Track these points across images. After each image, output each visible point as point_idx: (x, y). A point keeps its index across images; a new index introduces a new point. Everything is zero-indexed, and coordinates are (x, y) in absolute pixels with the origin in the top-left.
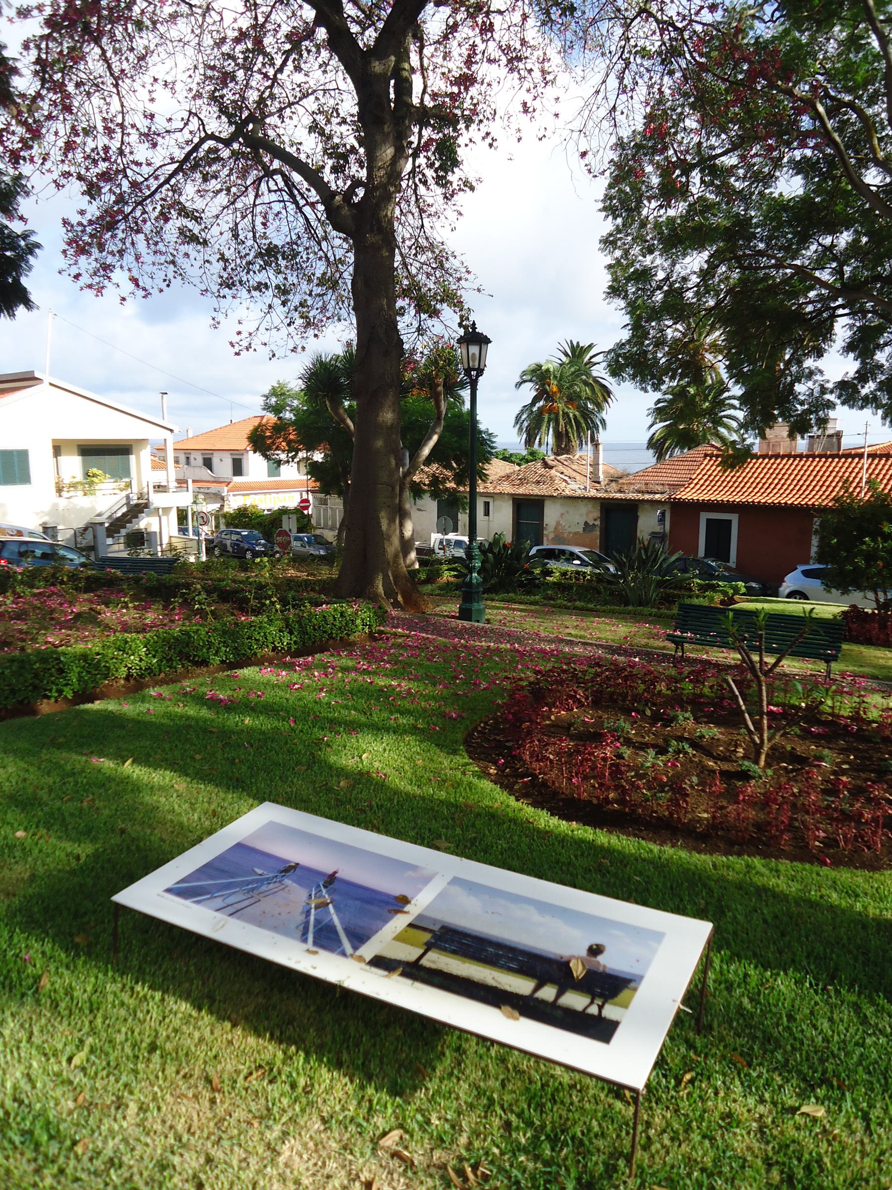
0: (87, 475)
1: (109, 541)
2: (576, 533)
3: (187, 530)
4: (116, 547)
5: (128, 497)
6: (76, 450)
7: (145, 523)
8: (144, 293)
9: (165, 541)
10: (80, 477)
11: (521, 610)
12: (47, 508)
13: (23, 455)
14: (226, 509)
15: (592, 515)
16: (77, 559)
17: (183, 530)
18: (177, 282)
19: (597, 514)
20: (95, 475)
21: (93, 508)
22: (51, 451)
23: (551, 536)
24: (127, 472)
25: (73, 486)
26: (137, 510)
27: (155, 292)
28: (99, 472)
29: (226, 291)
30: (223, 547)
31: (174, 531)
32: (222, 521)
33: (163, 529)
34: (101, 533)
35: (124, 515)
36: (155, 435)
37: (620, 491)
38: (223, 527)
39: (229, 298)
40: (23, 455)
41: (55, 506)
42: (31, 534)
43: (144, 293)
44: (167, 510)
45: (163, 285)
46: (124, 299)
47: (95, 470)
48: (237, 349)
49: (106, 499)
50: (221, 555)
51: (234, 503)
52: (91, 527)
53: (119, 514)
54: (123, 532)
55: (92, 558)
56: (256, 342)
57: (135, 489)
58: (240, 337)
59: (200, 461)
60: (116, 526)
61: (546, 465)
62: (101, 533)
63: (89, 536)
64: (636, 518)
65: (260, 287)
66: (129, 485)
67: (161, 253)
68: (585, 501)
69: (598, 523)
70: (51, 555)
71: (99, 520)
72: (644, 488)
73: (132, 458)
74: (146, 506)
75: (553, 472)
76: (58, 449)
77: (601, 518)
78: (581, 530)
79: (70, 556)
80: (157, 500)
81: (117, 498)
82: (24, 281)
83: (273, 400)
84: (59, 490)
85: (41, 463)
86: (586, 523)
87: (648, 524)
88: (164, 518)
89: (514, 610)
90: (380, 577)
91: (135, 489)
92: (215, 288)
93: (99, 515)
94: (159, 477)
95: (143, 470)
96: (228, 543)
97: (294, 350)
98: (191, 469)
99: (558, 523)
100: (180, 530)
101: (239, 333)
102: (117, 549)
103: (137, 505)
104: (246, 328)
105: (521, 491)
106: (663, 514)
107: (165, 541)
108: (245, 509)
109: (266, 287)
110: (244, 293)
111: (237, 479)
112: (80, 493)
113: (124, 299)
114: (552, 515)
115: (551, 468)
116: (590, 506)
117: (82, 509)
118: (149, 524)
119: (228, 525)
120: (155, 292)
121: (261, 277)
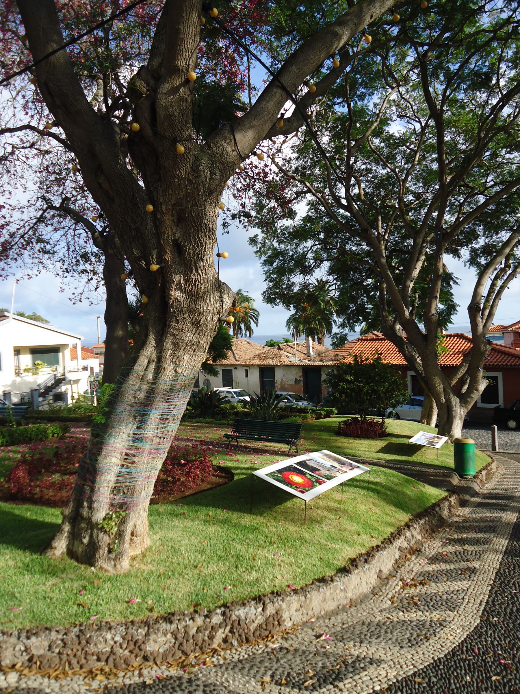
0: (34, 364)
2: (291, 385)
6: (29, 352)
8: (28, 277)
10: (30, 365)
11: (191, 426)
12: (9, 383)
15: (298, 374)
18: (43, 271)
19: (301, 374)
20: (38, 364)
21: (36, 382)
22: (12, 352)
23: (279, 387)
24: (57, 362)
25: (26, 370)
26: (58, 382)
29: (66, 274)
34: (36, 394)
35: (52, 385)
36: (71, 342)
37: (321, 361)
39: (69, 277)
41: (14, 381)
43: (28, 277)
45: (37, 273)
46: (18, 280)
47: (39, 362)
48: (73, 301)
49: (44, 376)
52: (32, 391)
56: (83, 297)
58: (74, 296)
60: (48, 389)
61: (280, 349)
62: (36, 394)
65: (84, 271)
67: (36, 258)
68: (295, 367)
69: (302, 379)
72: (333, 359)
73: (60, 354)
74: (64, 379)
75: (282, 352)
76: (18, 351)
77: (303, 376)
78: (294, 383)
84: (18, 374)
86: (296, 379)
89: (188, 426)
90: (435, 405)
92: (61, 273)
93: (39, 386)
99: (282, 379)
101: (74, 294)
102: (44, 405)
103: (59, 379)
105: (263, 363)
110: (76, 275)
113: (18, 280)
114: (279, 375)
115: (282, 350)
116: (297, 369)
117: (29, 382)
118: (67, 389)
120: (34, 276)
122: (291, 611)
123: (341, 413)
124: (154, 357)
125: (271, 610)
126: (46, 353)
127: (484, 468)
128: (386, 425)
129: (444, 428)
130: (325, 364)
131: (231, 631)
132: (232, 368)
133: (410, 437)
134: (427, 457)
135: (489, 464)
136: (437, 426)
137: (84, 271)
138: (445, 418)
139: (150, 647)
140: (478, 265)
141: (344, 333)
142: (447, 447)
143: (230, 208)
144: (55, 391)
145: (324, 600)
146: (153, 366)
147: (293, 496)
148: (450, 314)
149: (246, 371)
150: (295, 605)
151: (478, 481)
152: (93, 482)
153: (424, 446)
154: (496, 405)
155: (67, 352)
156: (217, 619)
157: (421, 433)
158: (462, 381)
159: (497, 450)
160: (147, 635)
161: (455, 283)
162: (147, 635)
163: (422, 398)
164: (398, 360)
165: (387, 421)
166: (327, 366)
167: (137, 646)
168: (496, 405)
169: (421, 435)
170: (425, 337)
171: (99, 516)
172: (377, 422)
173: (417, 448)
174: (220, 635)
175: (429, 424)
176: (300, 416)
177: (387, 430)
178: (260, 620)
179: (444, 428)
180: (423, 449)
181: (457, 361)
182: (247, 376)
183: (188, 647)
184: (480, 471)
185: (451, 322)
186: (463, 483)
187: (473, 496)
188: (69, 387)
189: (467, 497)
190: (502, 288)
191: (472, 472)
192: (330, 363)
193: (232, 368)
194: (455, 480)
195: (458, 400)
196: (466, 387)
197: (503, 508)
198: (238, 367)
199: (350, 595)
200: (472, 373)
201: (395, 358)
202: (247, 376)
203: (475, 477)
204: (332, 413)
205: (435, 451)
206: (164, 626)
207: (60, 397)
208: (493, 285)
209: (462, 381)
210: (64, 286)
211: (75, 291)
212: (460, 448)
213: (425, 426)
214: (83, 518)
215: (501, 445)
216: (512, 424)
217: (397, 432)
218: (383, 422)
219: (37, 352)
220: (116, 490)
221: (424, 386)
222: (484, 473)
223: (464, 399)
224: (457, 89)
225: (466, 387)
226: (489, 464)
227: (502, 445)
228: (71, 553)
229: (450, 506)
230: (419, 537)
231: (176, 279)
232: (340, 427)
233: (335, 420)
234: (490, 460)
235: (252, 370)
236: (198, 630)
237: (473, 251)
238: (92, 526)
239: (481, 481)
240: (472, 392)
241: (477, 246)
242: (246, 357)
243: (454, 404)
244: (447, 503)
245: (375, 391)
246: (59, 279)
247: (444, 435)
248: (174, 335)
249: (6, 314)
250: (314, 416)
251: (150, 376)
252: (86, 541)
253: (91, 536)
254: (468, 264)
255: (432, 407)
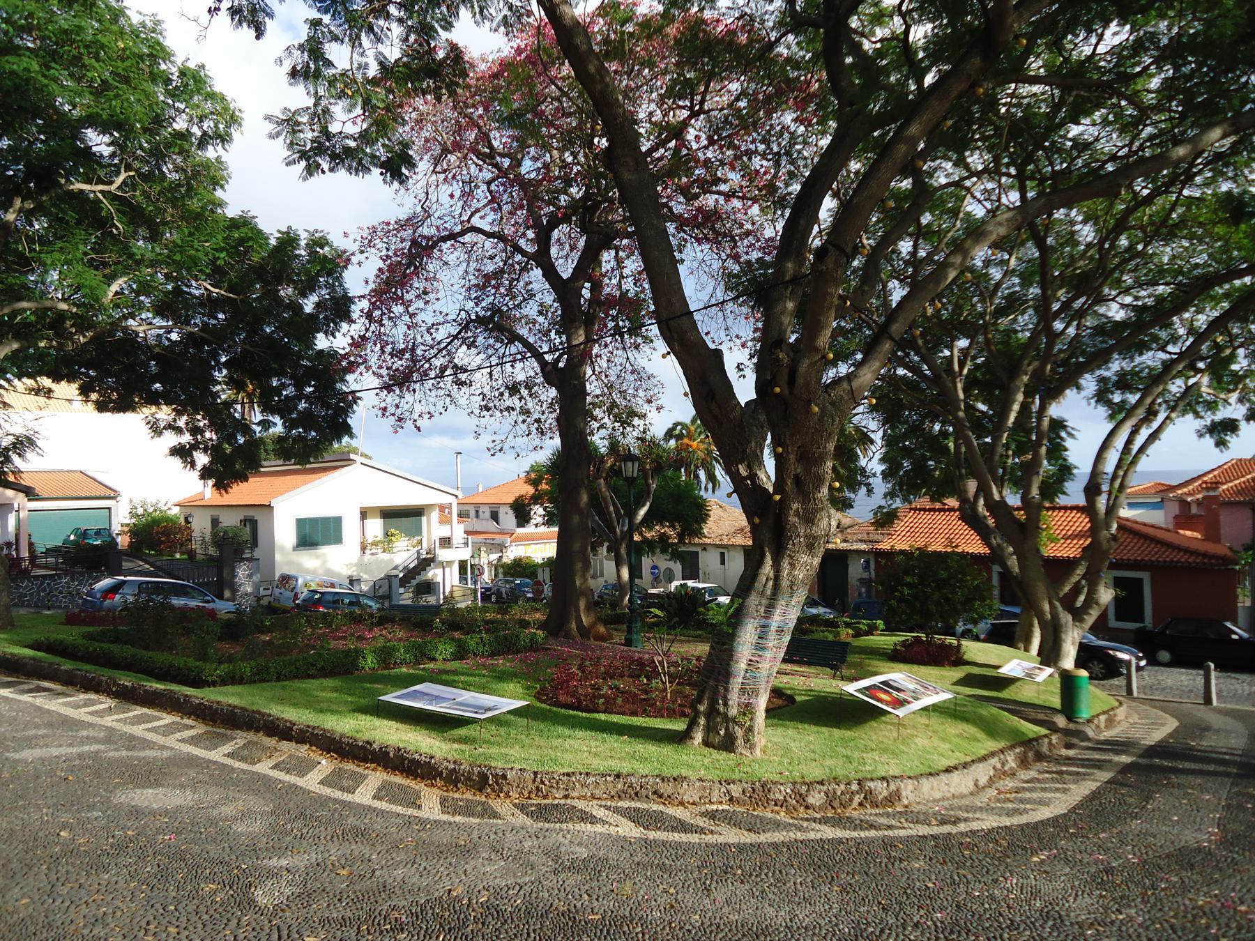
0: (386, 535)
1: (401, 590)
3: (466, 579)
4: (406, 596)
5: (418, 552)
7: (434, 574)
9: (448, 590)
10: (380, 537)
13: (337, 521)
14: (505, 560)
16: (375, 606)
17: (462, 578)
18: (451, 408)
24: (419, 532)
25: (375, 544)
27: (436, 414)
28: (396, 532)
30: (498, 593)
31: (456, 581)
32: (501, 570)
33: (447, 580)
34: (396, 582)
38: (501, 576)
40: (337, 521)
42: (341, 586)
44: (450, 563)
47: (393, 531)
49: (403, 554)
50: (497, 602)
51: (511, 554)
52: (389, 578)
53: (412, 565)
54: (414, 582)
55: (387, 604)
56: (506, 446)
57: (425, 546)
59: (488, 514)
60: (411, 574)
62: (396, 582)
63: (385, 588)
64: (847, 566)
65: (510, 409)
66: (420, 542)
70: (356, 601)
71: (395, 572)
72: (866, 538)
73: (424, 519)
74: (433, 560)
76: (364, 514)
79: (370, 603)
80: (443, 555)
81: (409, 553)
82: (349, 420)
83: (533, 476)
84: (363, 549)
85: (351, 529)
87: (856, 570)
88: (447, 570)
90: (1036, 622)
91: (425, 546)
92: (477, 412)
93: (396, 568)
94: (445, 531)
95: (433, 529)
96: (503, 590)
97: (535, 449)
98: (479, 521)
100: (460, 580)
102: (405, 597)
103: (425, 559)
104: (498, 438)
106: (867, 562)
107: (448, 590)
108: (520, 560)
109: (513, 409)
110: (498, 413)
111: (520, 531)
112: (380, 550)
118: (435, 575)
119: (505, 574)
120: (436, 414)
121: (509, 403)
122: (907, 789)
123: (890, 629)
124: (772, 575)
125: (893, 787)
126: (402, 517)
127: (1104, 713)
128: (963, 649)
129: (1049, 655)
130: (855, 547)
131: (865, 798)
132: (699, 549)
133: (999, 667)
134: (1025, 693)
135: (1113, 709)
136: (1039, 655)
137: (510, 409)
138: (1051, 643)
139: (810, 800)
140: (1109, 403)
141: (893, 507)
142: (1052, 683)
143: (741, 334)
144: (419, 578)
145: (932, 789)
146: (771, 583)
147: (885, 713)
148: (1064, 480)
149: (722, 555)
150: (910, 787)
151: (1093, 726)
152: (727, 683)
153: (1018, 679)
154: (1137, 625)
155: (435, 515)
156: (855, 787)
157: (1016, 661)
158: (1076, 590)
159: (1135, 694)
160: (808, 790)
161: (1070, 435)
162: (808, 790)
163: (1017, 610)
164: (974, 546)
165: (965, 643)
166: (860, 552)
167: (802, 798)
168: (1137, 625)
169: (1014, 663)
170: (1022, 527)
171: (733, 712)
172: (951, 644)
173: (1008, 682)
174: (857, 799)
175: (1027, 650)
176: (830, 632)
177: (965, 657)
178: (885, 793)
179: (1049, 655)
180: (1018, 684)
181: (1069, 550)
182: (723, 563)
183: (836, 804)
184: (1098, 715)
185: (1064, 493)
186: (1072, 726)
187: (1083, 741)
188: (439, 571)
189: (1075, 741)
190: (1142, 449)
191: (1085, 714)
192: (863, 547)
193: (699, 549)
194: (1061, 721)
195: (1070, 617)
196: (1082, 598)
197: (1117, 752)
198: (708, 548)
199: (952, 790)
200: (1092, 578)
201: (974, 546)
202: (723, 563)
203: (1089, 721)
204: (876, 628)
205: (1035, 687)
206: (819, 787)
207: (428, 587)
208: (1129, 442)
209: (1076, 590)
210: (480, 430)
211: (494, 437)
212: (1068, 684)
213: (1021, 653)
214: (718, 713)
215: (1142, 688)
216: (1164, 656)
217: (980, 660)
218: (959, 646)
219: (389, 514)
220: (743, 691)
221: (1020, 594)
222: (1103, 718)
223: (1078, 615)
224: (1011, 768)
225: (1082, 598)
226: (1113, 709)
227: (1144, 687)
228: (706, 743)
229: (1050, 744)
230: (1013, 765)
231: (795, 506)
232: (895, 650)
233: (886, 641)
234: (1117, 704)
235: (732, 553)
236: (842, 793)
237: (1102, 380)
238: (727, 719)
239: (1098, 727)
240: (1090, 607)
241: (1107, 374)
242: (720, 532)
243: (1063, 621)
244: (1046, 740)
245: (948, 600)
246: (475, 421)
247: (1049, 666)
248: (791, 557)
249: (352, 456)
250: (851, 631)
251: (769, 592)
252: (722, 733)
253: (727, 729)
254: (1093, 401)
255: (1031, 625)
